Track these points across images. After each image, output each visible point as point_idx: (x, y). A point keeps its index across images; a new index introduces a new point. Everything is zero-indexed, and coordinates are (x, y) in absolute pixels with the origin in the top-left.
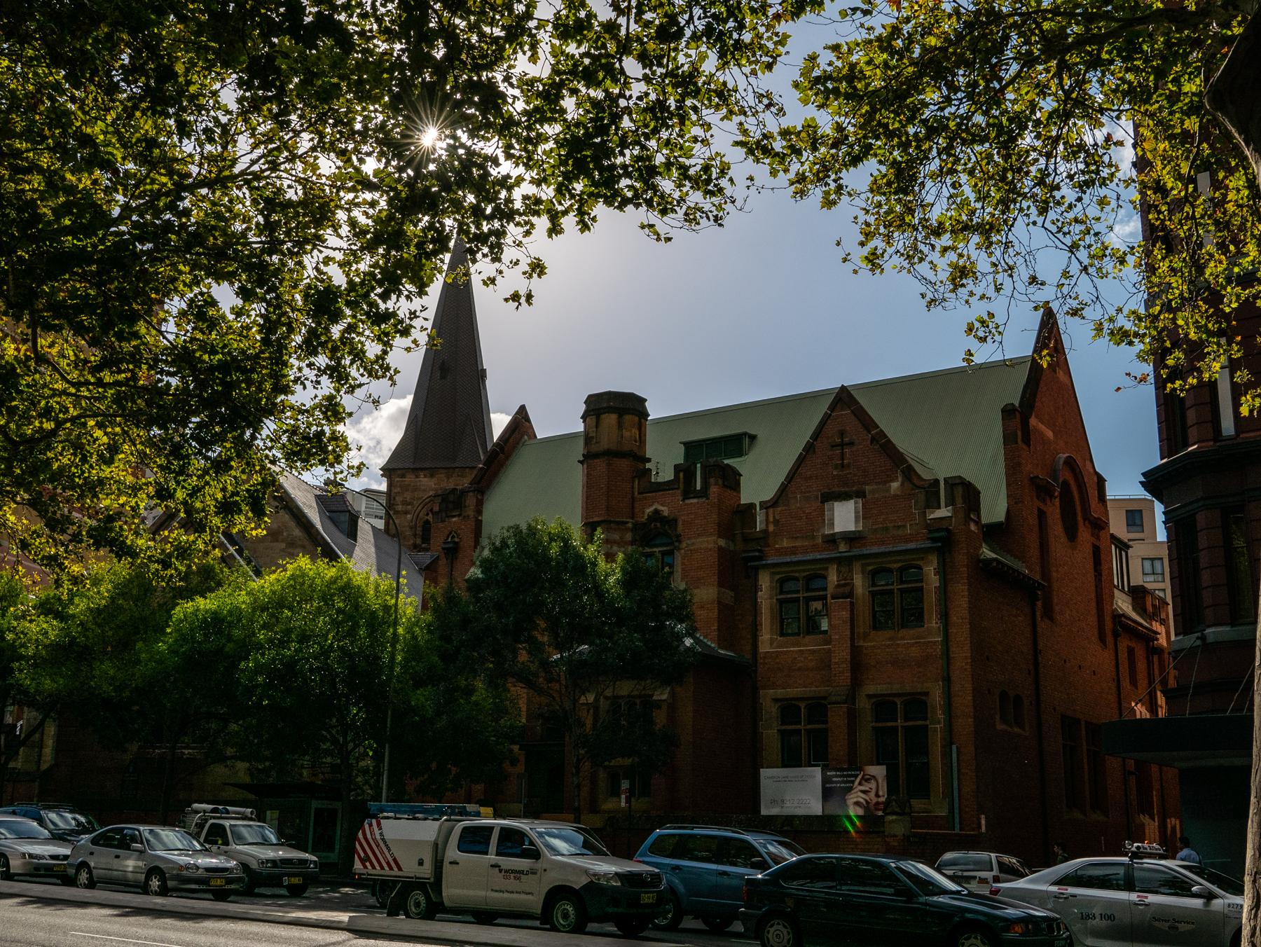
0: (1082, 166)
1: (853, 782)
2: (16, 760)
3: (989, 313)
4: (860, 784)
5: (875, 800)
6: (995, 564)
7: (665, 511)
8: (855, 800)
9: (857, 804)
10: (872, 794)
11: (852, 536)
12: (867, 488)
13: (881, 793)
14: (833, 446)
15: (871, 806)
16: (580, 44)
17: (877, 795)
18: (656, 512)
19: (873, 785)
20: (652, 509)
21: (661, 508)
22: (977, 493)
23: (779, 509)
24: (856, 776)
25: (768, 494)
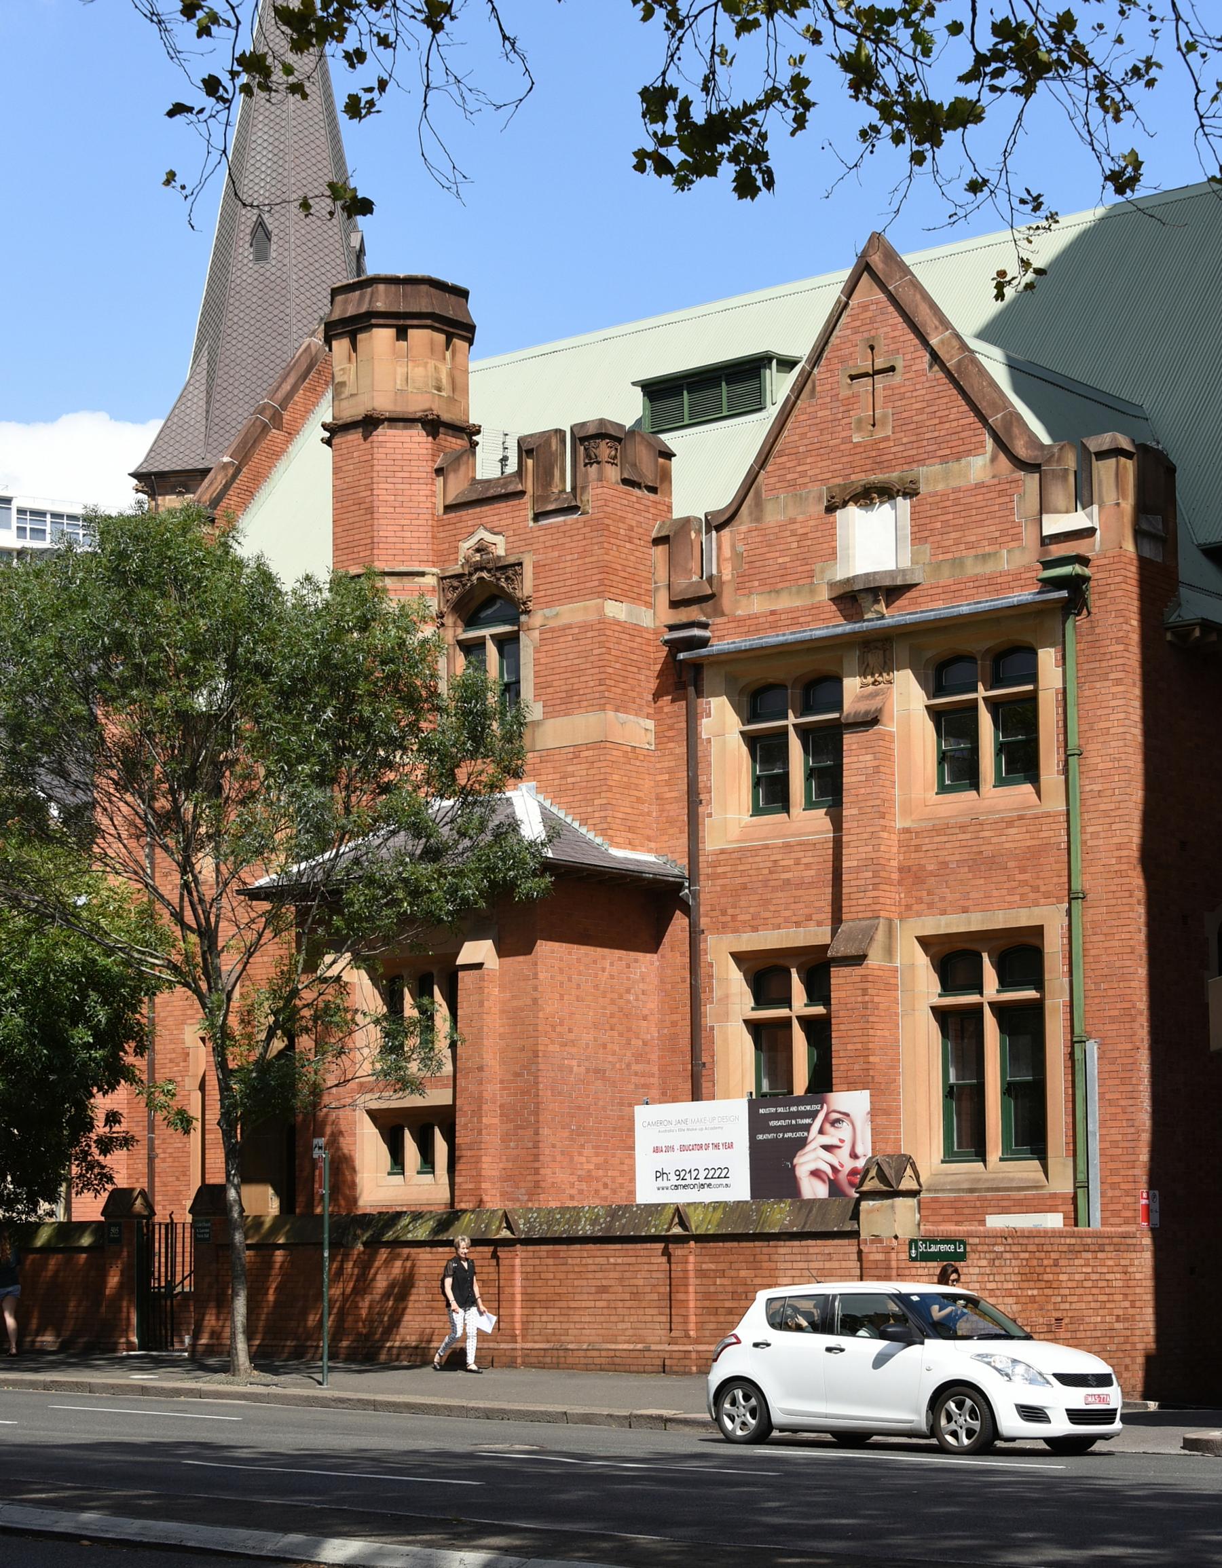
0: (111, 877)
1: (807, 1128)
2: (986, 690)
3: (1154, 80)
4: (821, 1131)
5: (849, 1164)
6: (1197, 633)
7: (500, 547)
8: (812, 1167)
9: (816, 1173)
10: (844, 1152)
11: (887, 582)
12: (923, 471)
13: (859, 1150)
14: (852, 378)
15: (843, 1176)
16: (45, 963)
17: (854, 1156)
18: (481, 549)
19: (844, 1131)
20: (472, 542)
21: (489, 537)
22: (1171, 470)
23: (744, 528)
24: (813, 1115)
25: (721, 497)
